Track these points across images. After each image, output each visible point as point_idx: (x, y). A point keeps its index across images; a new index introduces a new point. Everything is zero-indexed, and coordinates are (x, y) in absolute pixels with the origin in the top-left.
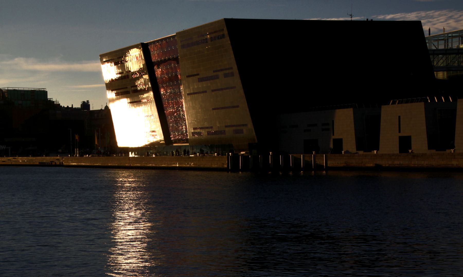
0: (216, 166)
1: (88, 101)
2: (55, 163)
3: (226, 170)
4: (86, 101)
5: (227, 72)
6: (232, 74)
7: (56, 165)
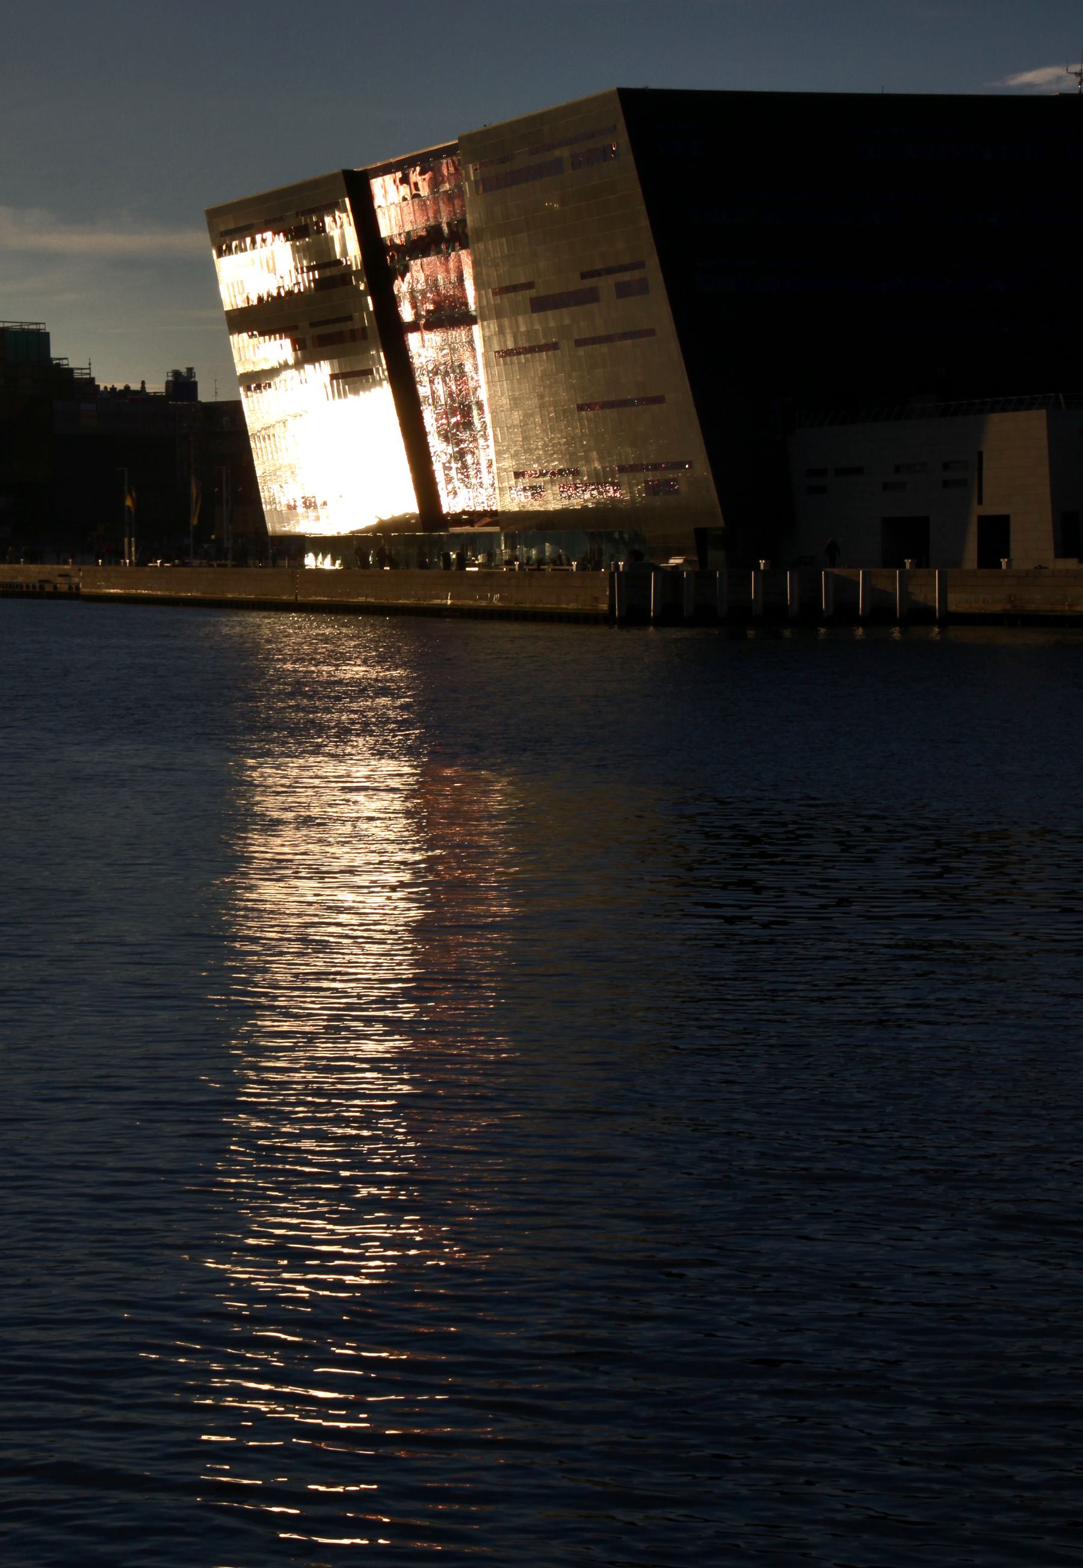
0: (572, 606)
1: (190, 370)
2: (55, 587)
3: (606, 619)
4: (183, 370)
5: (626, 277)
6: (642, 287)
7: (56, 595)
